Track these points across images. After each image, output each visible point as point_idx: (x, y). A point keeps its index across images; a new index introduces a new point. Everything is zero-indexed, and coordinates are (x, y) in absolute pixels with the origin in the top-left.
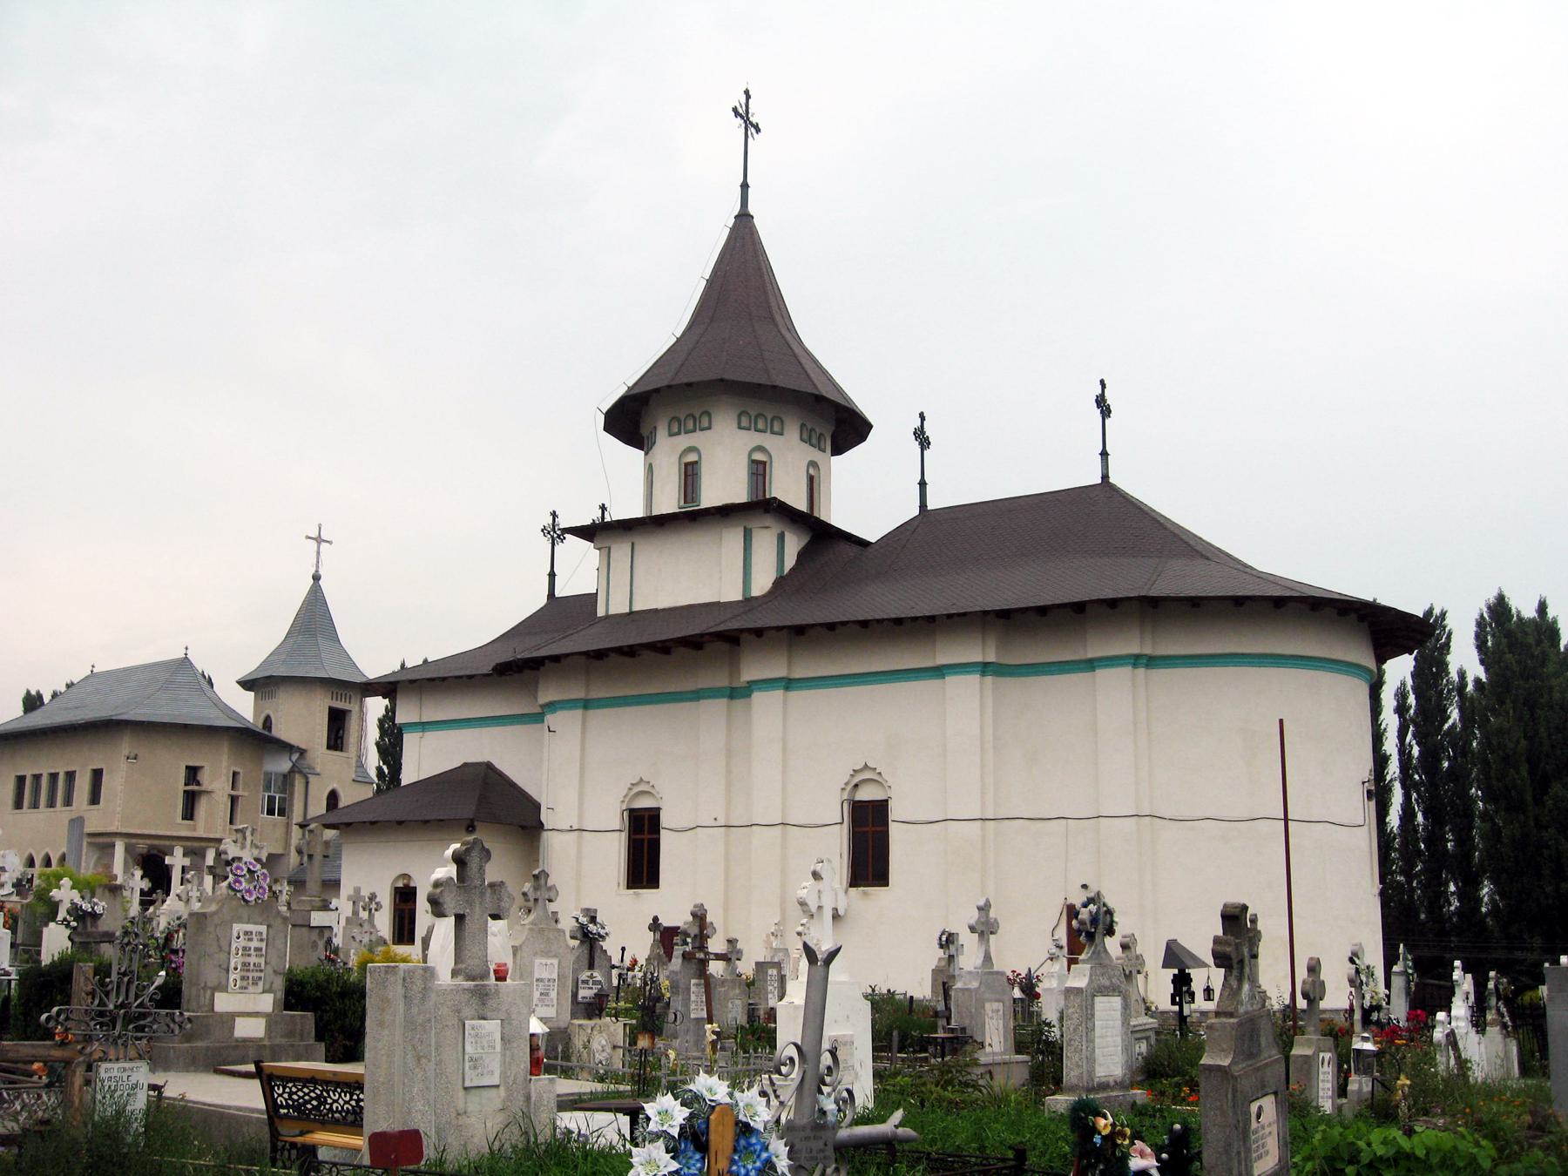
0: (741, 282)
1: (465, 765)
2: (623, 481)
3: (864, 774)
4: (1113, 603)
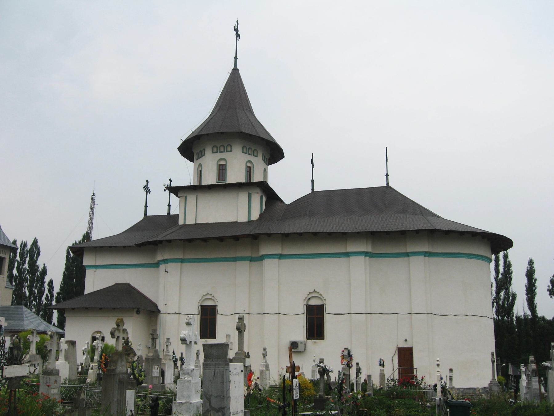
0: (234, 94)
1: (117, 284)
2: (185, 173)
3: (315, 294)
4: (417, 232)
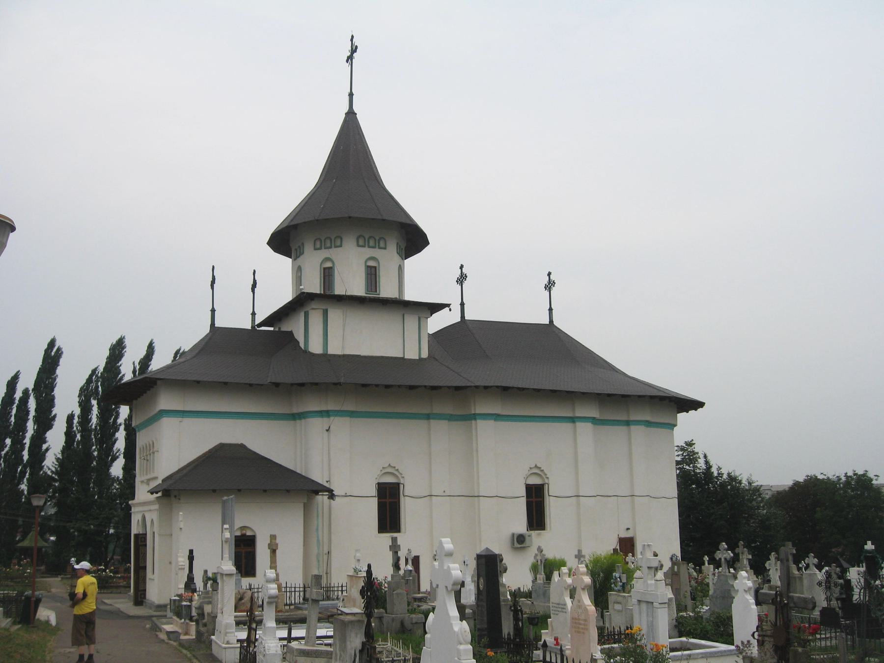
0: (350, 153)
